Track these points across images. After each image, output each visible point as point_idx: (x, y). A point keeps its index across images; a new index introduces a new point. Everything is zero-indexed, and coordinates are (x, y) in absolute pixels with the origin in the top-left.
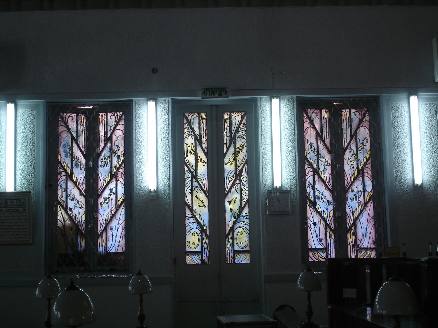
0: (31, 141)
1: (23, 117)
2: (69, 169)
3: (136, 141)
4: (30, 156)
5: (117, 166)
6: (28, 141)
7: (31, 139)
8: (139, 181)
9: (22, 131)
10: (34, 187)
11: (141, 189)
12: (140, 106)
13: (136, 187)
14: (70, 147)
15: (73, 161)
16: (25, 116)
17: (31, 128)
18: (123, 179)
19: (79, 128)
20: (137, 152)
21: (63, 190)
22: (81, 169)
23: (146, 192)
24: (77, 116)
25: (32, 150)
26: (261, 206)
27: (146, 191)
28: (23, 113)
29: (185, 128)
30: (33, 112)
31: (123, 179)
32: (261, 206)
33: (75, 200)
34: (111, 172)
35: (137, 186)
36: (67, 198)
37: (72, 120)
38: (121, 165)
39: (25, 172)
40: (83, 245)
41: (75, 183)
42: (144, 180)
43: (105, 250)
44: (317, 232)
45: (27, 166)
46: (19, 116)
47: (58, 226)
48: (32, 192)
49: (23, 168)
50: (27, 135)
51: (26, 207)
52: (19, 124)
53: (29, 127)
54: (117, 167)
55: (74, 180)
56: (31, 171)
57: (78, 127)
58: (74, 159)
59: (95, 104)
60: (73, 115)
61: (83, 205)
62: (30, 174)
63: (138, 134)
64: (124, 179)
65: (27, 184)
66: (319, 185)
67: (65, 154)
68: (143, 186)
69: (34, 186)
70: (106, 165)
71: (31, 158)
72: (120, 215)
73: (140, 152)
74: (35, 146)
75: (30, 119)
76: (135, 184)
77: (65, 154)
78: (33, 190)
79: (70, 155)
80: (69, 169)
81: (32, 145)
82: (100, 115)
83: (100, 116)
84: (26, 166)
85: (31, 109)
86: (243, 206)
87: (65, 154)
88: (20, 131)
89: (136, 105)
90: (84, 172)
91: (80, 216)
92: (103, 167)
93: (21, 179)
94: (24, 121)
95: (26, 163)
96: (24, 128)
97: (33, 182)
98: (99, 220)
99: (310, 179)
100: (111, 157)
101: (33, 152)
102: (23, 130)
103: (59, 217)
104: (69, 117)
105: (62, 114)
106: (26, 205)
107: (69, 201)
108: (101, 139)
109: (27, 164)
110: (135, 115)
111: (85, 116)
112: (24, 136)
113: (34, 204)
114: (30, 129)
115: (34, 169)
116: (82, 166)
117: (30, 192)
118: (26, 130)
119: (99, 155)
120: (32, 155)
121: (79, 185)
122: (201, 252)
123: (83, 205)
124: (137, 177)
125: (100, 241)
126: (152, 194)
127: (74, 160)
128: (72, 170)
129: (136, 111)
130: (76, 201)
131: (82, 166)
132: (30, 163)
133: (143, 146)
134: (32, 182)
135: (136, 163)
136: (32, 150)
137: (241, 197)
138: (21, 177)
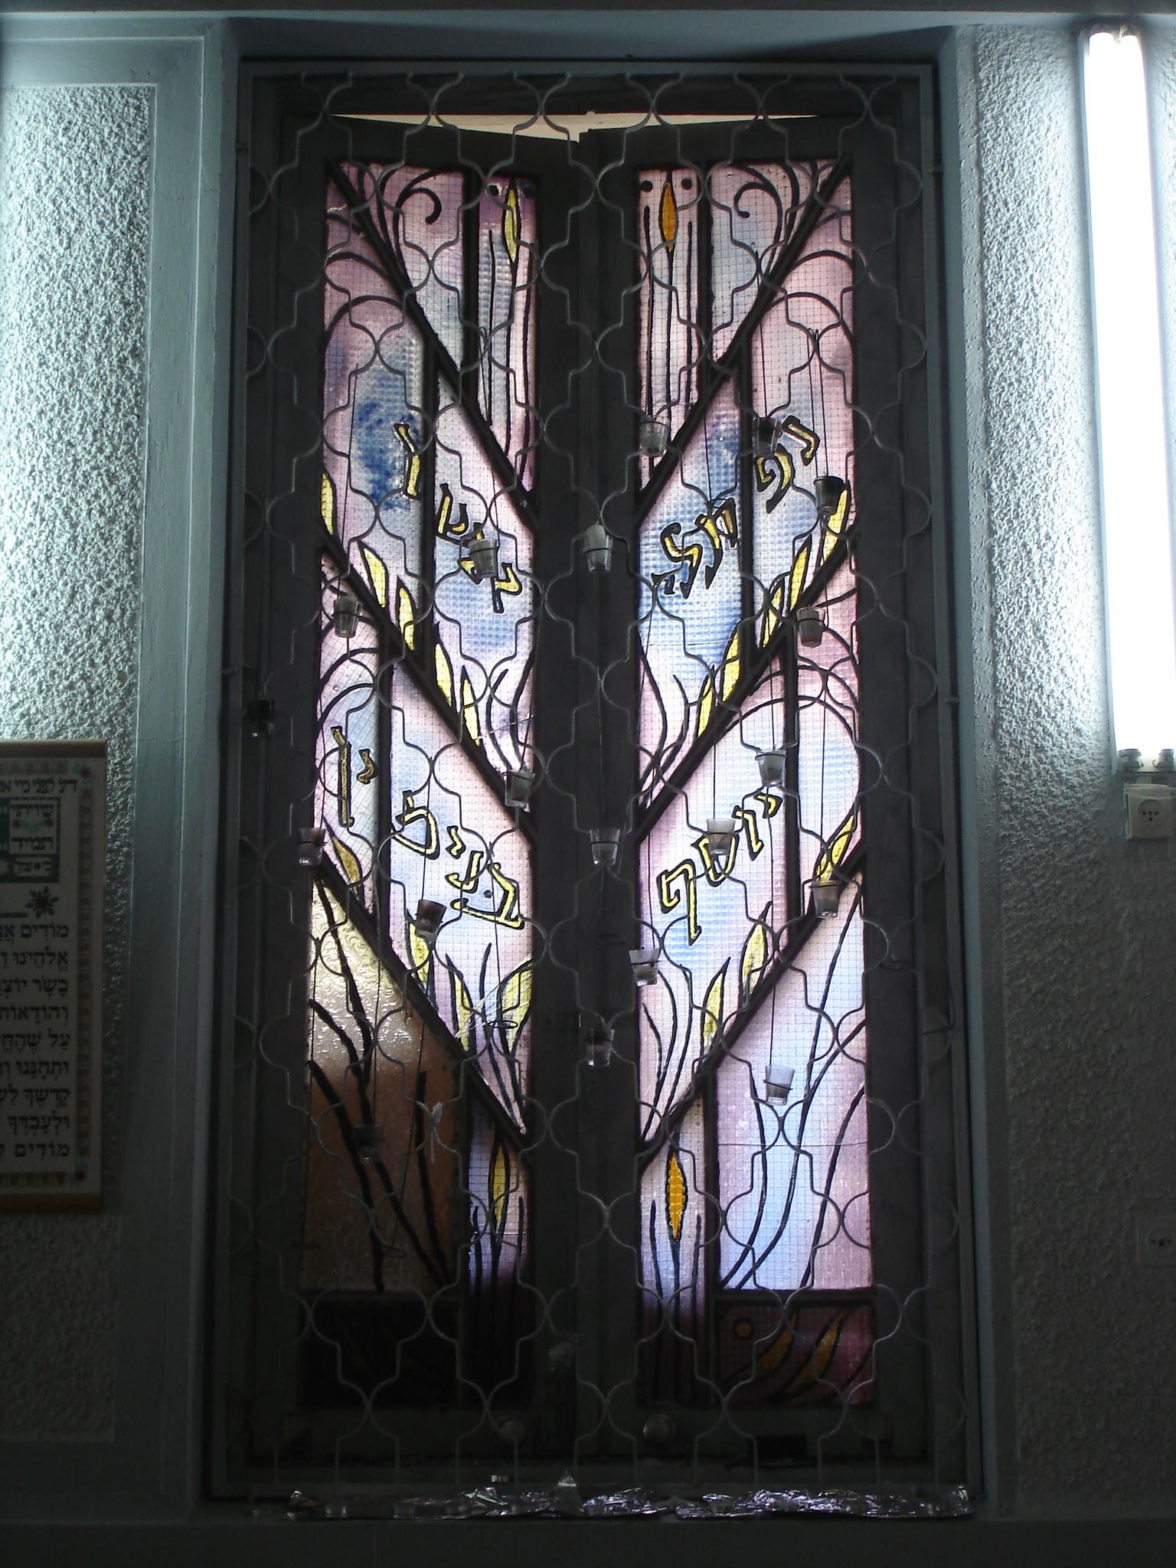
0: (108, 340)
1: (47, 143)
2: (405, 601)
3: (987, 353)
4: (101, 457)
5: (796, 586)
6: (83, 338)
7: (109, 322)
8: (1020, 684)
9: (35, 255)
10: (129, 718)
11: (1039, 749)
12: (1008, 77)
13: (994, 735)
14: (415, 431)
15: (438, 540)
16: (64, 140)
17: (117, 233)
18: (848, 688)
19: (484, 281)
20: (1001, 442)
21: (357, 765)
22: (499, 608)
23: (1078, 774)
24: (470, 192)
25: (117, 405)
27: (1082, 768)
28: (51, 114)
29: (854, 597)
30: (138, 108)
31: (848, 688)
33: (449, 849)
34: (744, 629)
35: (1005, 724)
36: (384, 827)
37: (430, 220)
38: (826, 573)
39: (53, 588)
40: (512, 1227)
41: (448, 715)
42: (1061, 679)
43: (701, 1275)
45: (74, 538)
46: (21, 138)
47: (313, 1065)
48: (114, 756)
49: (36, 554)
50: (80, 291)
51: (54, 878)
52: (17, 200)
53: (101, 223)
54: (795, 594)
55: (440, 690)
56: (109, 584)
57: (477, 277)
58: (443, 521)
59: (628, 75)
60: (435, 183)
61: (511, 895)
62: (96, 602)
63: (999, 297)
64: (853, 682)
65: (71, 687)
67: (377, 477)
68: (1051, 729)
69: (130, 711)
70: (700, 576)
71: (112, 478)
72: (824, 979)
73: (1022, 443)
74: (141, 378)
75: (107, 159)
76: (989, 708)
77: (371, 476)
78: (122, 736)
79: (411, 490)
80: (405, 601)
81: (121, 367)
82: (648, 186)
83: (651, 193)
84: (64, 539)
85: (115, 86)
87: (373, 481)
88: (25, 253)
89: (976, 70)
90: (808, 364)
91: (492, 983)
92: (678, 592)
93: (16, 647)
94: (57, 176)
95: (66, 514)
96: (59, 230)
97: (122, 677)
98: (649, 1018)
100: (742, 509)
101: (128, 425)
102: (43, 244)
103: (327, 987)
104: (407, 194)
105: (351, 171)
106: (56, 858)
107: (399, 853)
108: (658, 371)
109: (74, 526)
110: (974, 146)
111: (528, 193)
112: (56, 298)
113: (127, 855)
114: (103, 238)
115: (133, 565)
116: (508, 580)
117: (98, 751)
118: (69, 247)
119: (646, 500)
120: (115, 449)
121: (484, 731)
123: (517, 891)
124: (1002, 655)
125: (653, 1192)
126: (1143, 792)
127: (441, 530)
128: (425, 603)
129: (980, 116)
130: (457, 857)
131: (504, 585)
132: (102, 513)
133: (1044, 399)
134: (109, 674)
135: (992, 532)
136: (117, 405)
138: (20, 627)
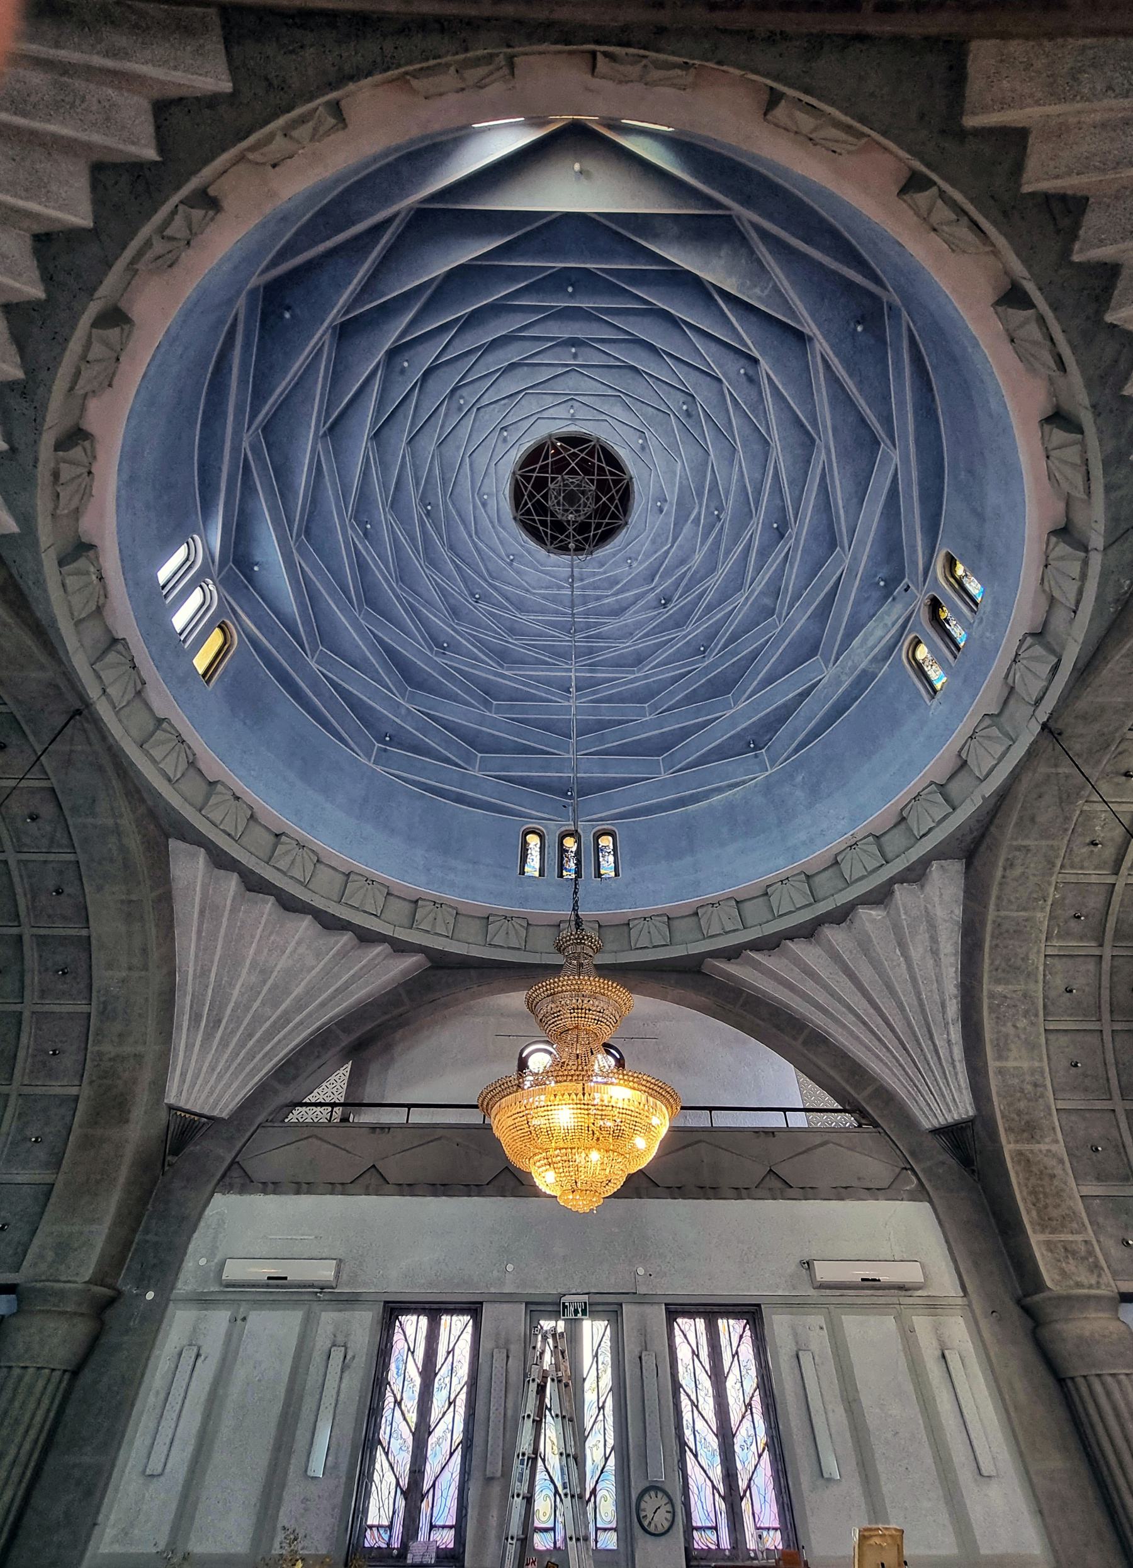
26: (366, 266)
32: (366, 266)
44: (703, 1500)
66: (700, 1425)
86: (607, 1455)
99: (687, 1416)
122: (553, 1529)
137: (605, 1441)
